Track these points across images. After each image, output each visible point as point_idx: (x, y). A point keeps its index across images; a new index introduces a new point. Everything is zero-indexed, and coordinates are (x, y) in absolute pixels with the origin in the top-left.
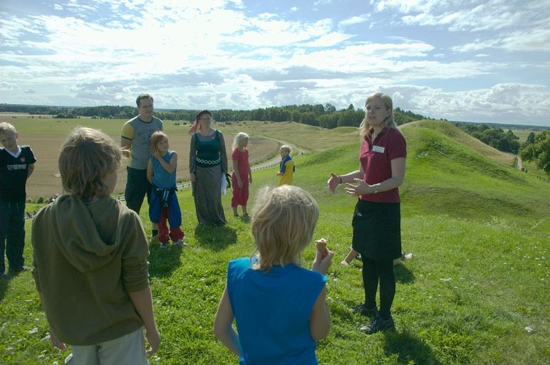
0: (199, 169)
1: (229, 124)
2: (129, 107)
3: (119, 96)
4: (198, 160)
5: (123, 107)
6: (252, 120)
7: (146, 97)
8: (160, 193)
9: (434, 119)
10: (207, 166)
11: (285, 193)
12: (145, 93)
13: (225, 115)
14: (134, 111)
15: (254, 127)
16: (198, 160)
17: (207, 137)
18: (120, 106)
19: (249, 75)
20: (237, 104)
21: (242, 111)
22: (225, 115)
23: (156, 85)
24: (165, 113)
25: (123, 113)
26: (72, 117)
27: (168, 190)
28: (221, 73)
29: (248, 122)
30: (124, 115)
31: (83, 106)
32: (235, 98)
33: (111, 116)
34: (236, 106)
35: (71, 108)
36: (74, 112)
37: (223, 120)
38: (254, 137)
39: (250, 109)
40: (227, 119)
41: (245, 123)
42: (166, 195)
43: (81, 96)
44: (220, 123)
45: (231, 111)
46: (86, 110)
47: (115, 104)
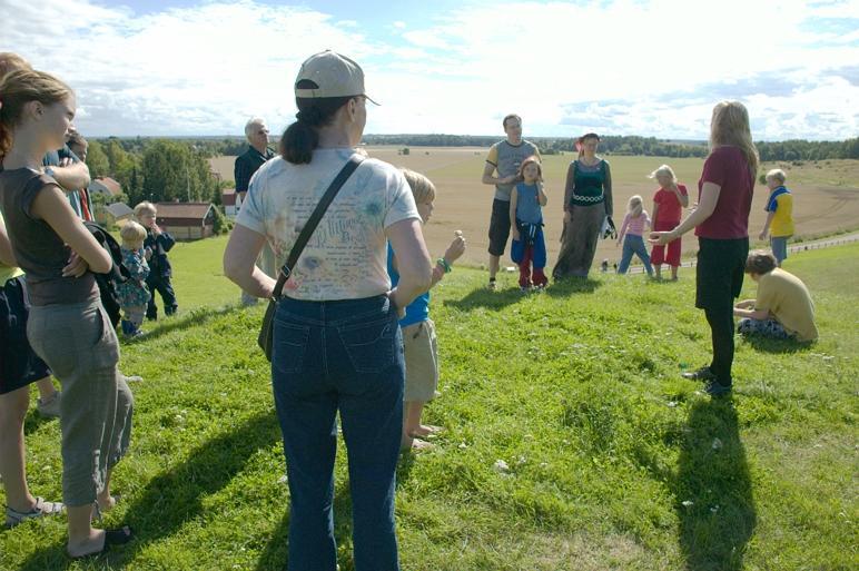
0: (579, 209)
1: (799, 165)
2: (637, 138)
3: (618, 120)
4: (576, 197)
5: (626, 138)
6: (843, 157)
7: (511, 117)
8: (527, 228)
9: (668, 141)
10: (589, 204)
11: (214, 178)
12: (507, 115)
13: (793, 150)
14: (643, 143)
15: (846, 171)
16: (576, 197)
17: (591, 167)
18: (623, 136)
19: (846, 77)
20: (815, 130)
21: (826, 143)
22: (793, 150)
23: (680, 102)
24: (691, 146)
25: (625, 147)
26: (553, 154)
27: (534, 225)
28: (791, 78)
29: (837, 162)
30: (628, 150)
31: (570, 137)
32: (811, 119)
33: (608, 151)
34: (816, 134)
35: (553, 139)
36: (555, 146)
37: (790, 158)
38: (843, 187)
39: (842, 139)
40: (798, 157)
41: (828, 163)
42: (532, 230)
43: (566, 122)
44: (783, 163)
45: (806, 142)
46: (848, 147)
47: (615, 133)
